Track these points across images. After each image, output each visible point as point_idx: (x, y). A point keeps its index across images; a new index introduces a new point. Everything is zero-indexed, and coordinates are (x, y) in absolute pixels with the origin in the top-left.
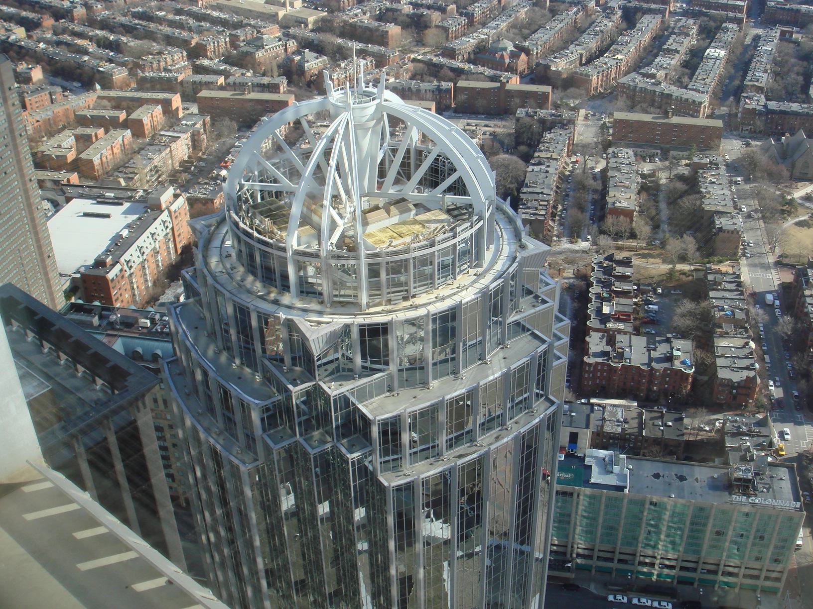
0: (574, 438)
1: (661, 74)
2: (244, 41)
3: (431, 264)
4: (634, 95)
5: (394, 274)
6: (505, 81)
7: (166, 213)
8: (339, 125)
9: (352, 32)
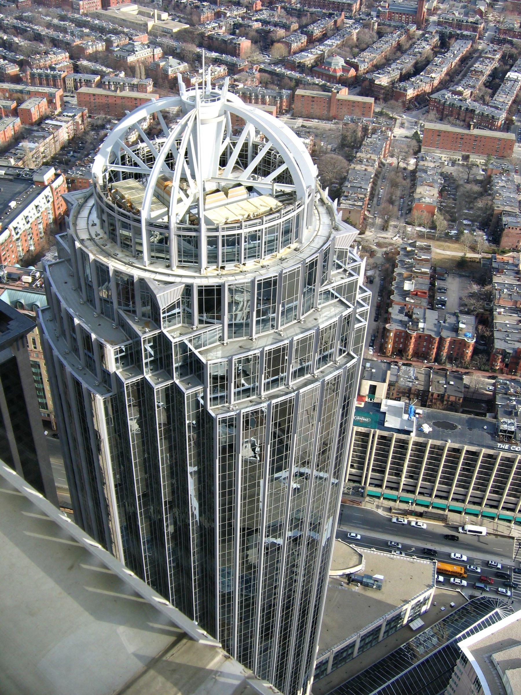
0: (373, 389)
1: (467, 93)
2: (118, 46)
3: (259, 240)
4: (443, 109)
5: (231, 246)
6: (336, 91)
8: (188, 120)
9: (211, 43)
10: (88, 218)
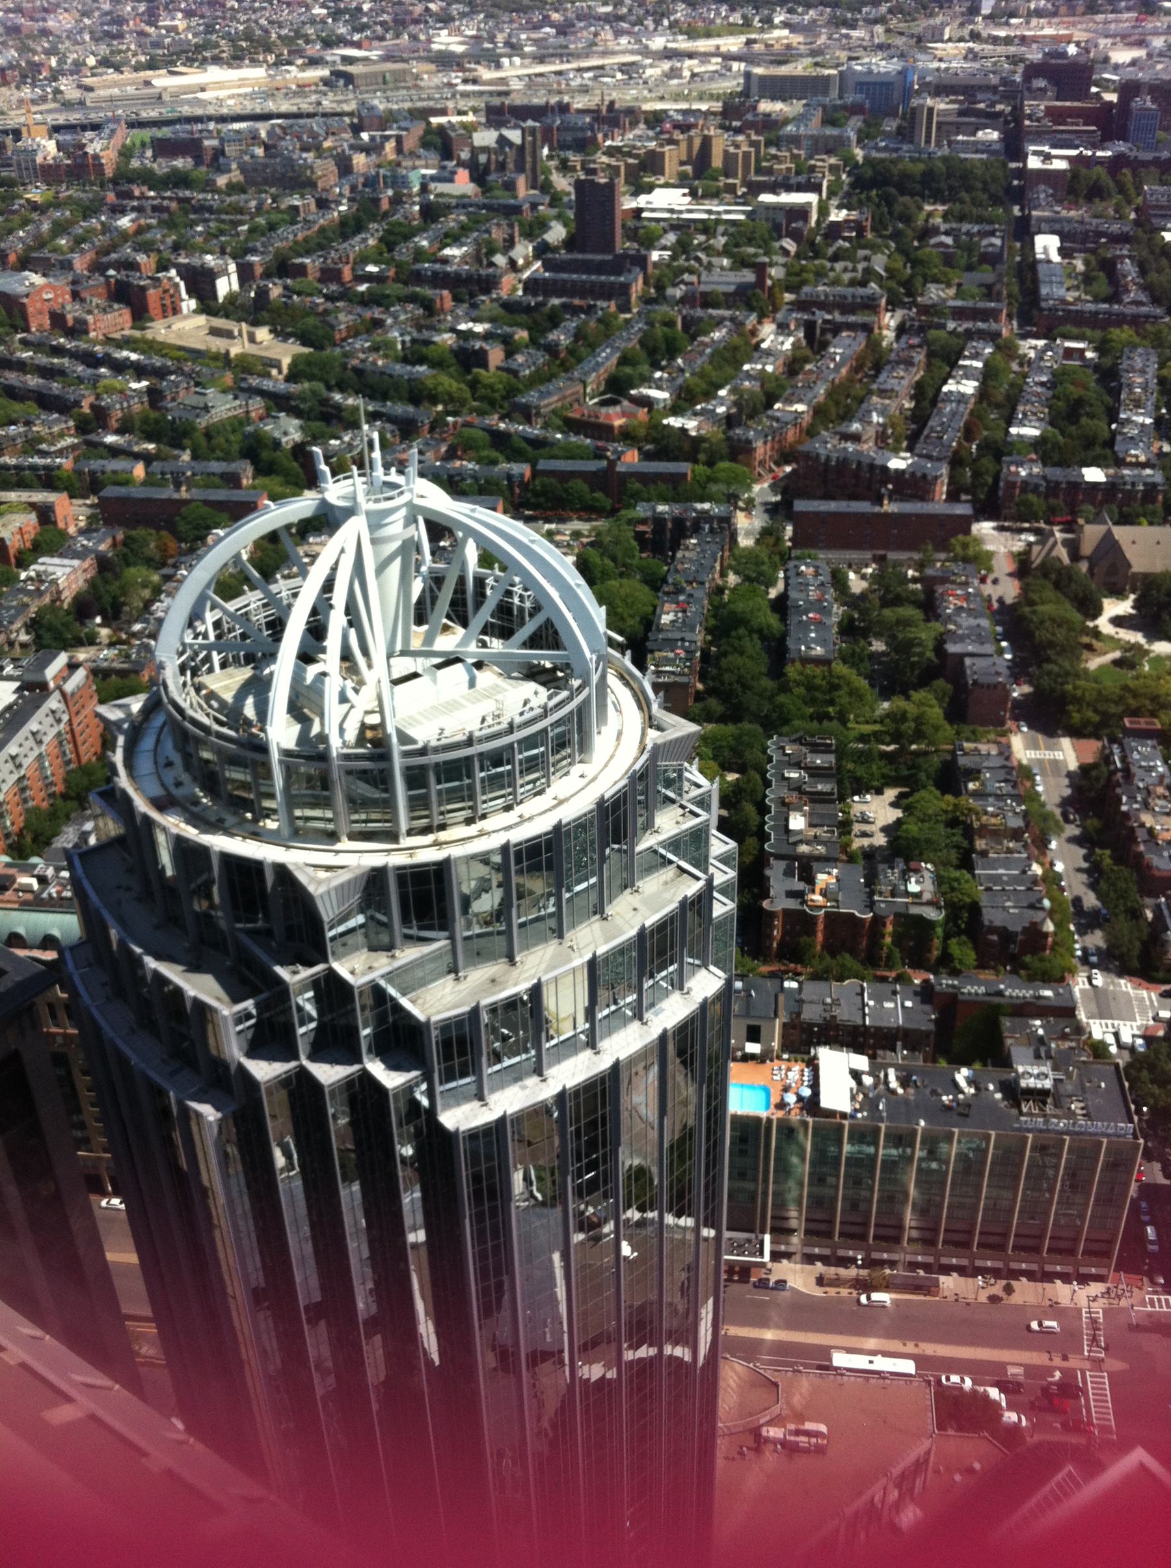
7: (57, 695)
10: (155, 750)
